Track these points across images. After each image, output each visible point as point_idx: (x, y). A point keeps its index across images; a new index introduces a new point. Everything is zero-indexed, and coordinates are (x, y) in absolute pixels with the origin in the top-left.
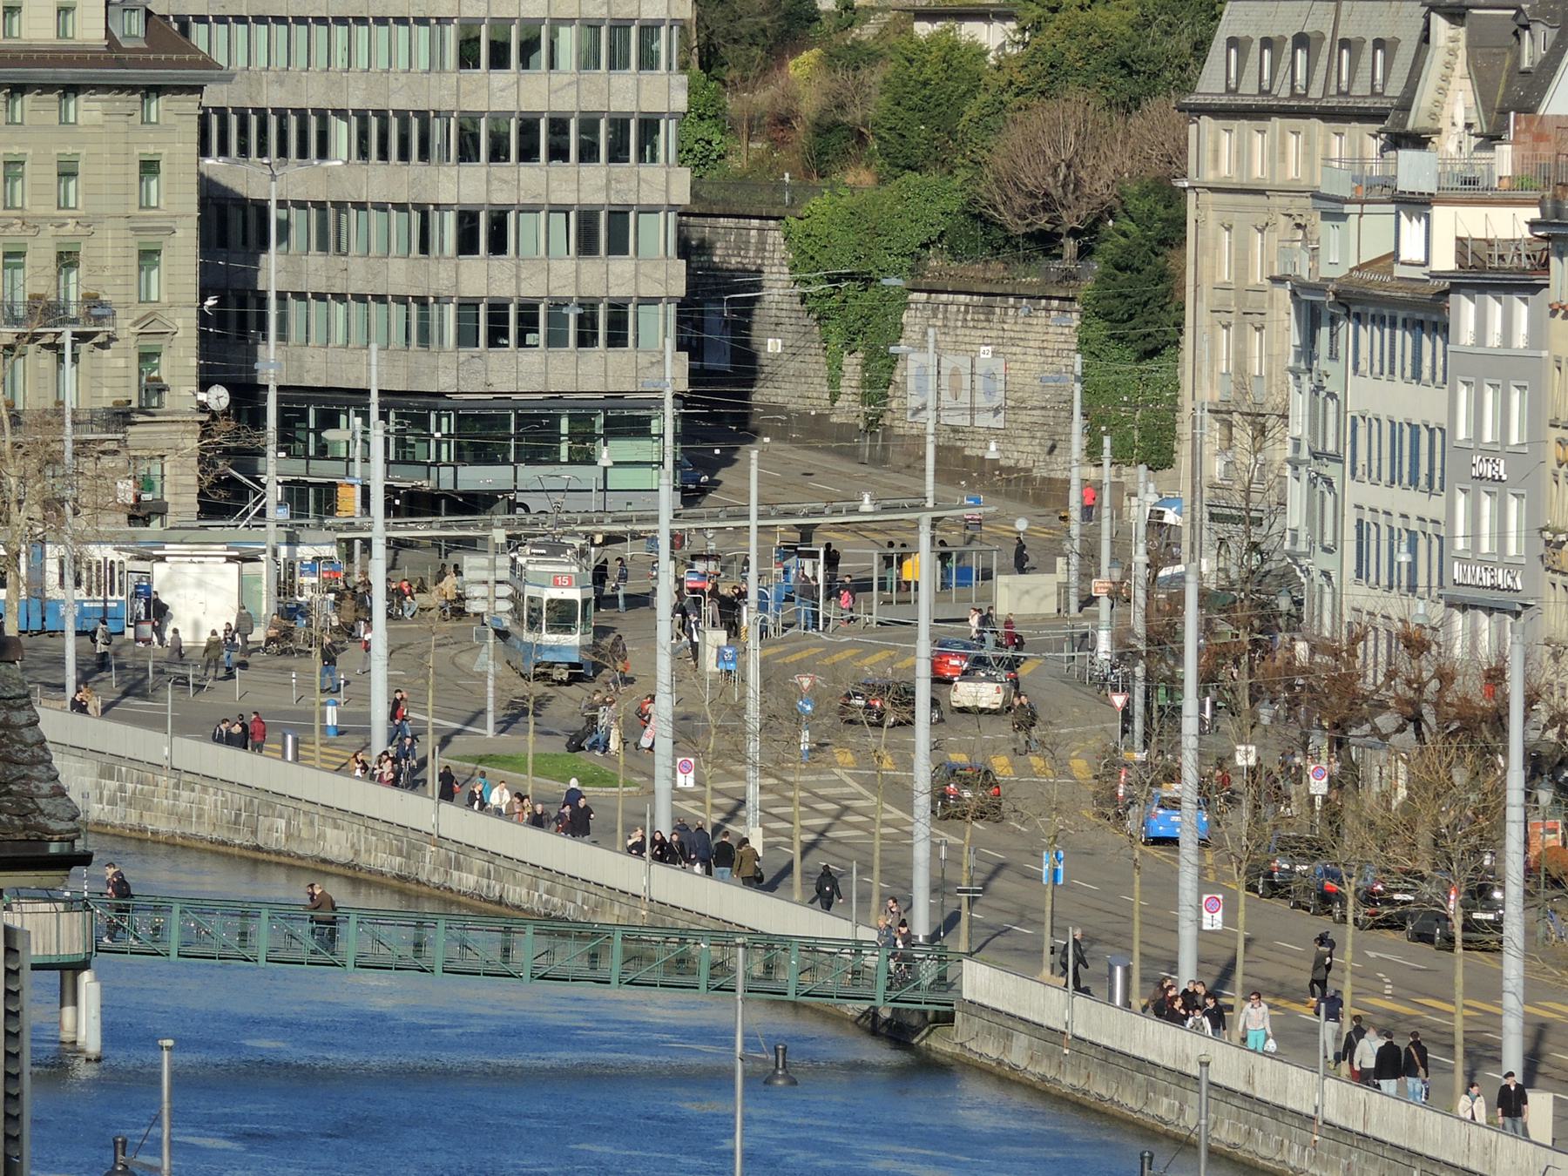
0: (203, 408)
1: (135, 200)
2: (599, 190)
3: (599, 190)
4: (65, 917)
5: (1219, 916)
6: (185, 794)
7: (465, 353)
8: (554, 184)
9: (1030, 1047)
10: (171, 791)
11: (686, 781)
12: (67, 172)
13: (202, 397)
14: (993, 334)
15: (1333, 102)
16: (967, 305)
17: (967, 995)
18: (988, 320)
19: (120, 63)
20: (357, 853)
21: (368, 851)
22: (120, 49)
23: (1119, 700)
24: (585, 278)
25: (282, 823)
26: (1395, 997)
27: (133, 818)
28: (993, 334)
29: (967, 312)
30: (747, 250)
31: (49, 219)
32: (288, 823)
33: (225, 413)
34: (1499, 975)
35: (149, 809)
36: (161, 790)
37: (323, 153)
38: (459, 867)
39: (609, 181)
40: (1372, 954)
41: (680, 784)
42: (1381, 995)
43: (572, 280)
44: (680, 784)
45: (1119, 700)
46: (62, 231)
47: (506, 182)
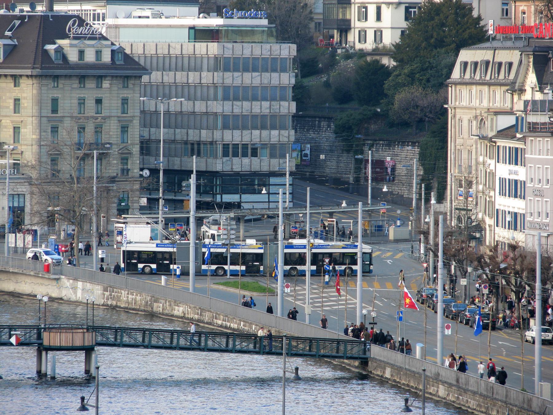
0: (141, 176)
1: (120, 111)
2: (267, 108)
3: (267, 108)
4: (86, 334)
5: (450, 330)
6: (130, 296)
7: (225, 159)
8: (253, 107)
9: (391, 371)
10: (126, 295)
11: (448, 332)
12: (99, 101)
13: (141, 173)
14: (391, 153)
15: (493, 81)
16: (383, 144)
17: (372, 356)
18: (389, 149)
19: (116, 69)
20: (184, 314)
21: (188, 314)
22: (116, 64)
23: (425, 265)
24: (263, 135)
25: (161, 305)
26: (507, 356)
27: (114, 303)
28: (391, 153)
29: (383, 146)
30: (315, 127)
31: (92, 117)
32: (163, 305)
33: (150, 176)
34: (534, 348)
35: (119, 301)
36: (123, 295)
37: (500, 178)
38: (216, 318)
39: (270, 106)
40: (500, 343)
41: (446, 333)
42: (502, 355)
43: (259, 136)
44: (446, 333)
45: (425, 265)
46: (97, 121)
47: (238, 106)
